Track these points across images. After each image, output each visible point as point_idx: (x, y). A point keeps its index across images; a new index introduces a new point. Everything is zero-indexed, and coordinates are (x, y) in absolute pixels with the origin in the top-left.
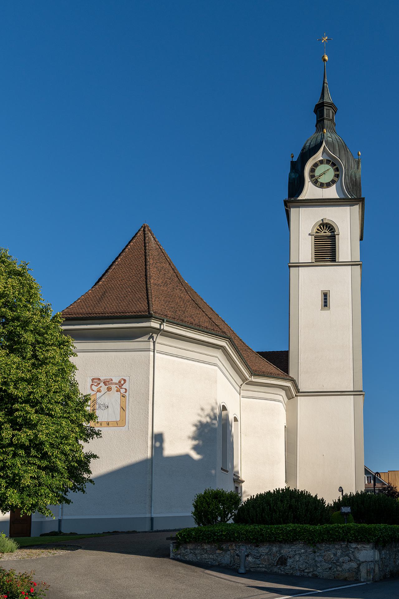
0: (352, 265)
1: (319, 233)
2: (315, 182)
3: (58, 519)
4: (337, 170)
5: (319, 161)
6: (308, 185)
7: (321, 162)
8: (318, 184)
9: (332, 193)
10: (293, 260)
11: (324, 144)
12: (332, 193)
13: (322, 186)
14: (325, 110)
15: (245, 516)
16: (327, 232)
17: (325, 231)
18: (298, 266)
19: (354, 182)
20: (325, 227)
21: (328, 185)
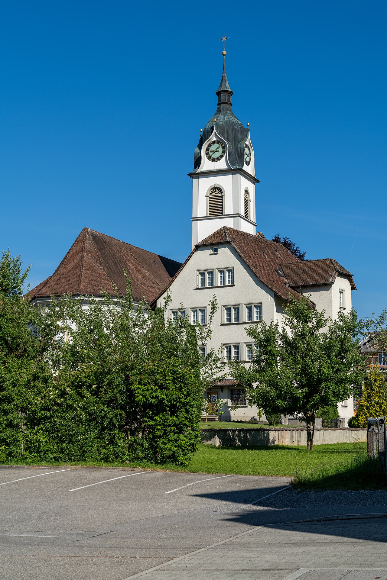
0: (233, 217)
1: (212, 194)
2: (209, 158)
3: (348, 405)
4: (223, 148)
5: (212, 142)
6: (205, 160)
7: (213, 143)
8: (211, 159)
9: (222, 164)
10: (194, 215)
11: (215, 130)
12: (222, 164)
13: (214, 160)
14: (222, 96)
15: (276, 402)
16: (218, 193)
17: (216, 192)
18: (198, 220)
19: (239, 152)
20: (216, 189)
21: (218, 159)
